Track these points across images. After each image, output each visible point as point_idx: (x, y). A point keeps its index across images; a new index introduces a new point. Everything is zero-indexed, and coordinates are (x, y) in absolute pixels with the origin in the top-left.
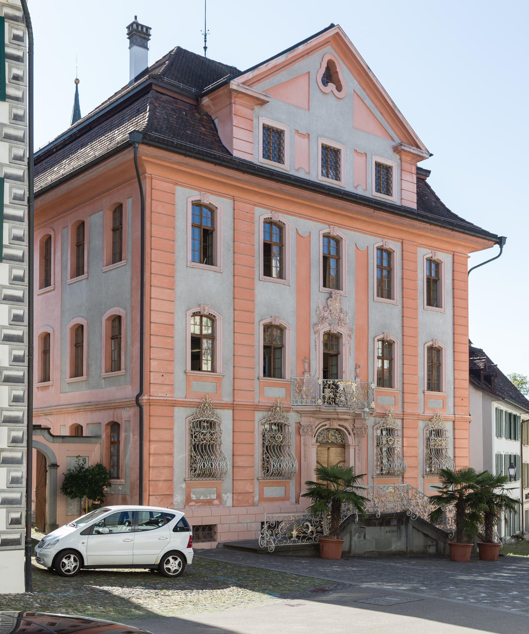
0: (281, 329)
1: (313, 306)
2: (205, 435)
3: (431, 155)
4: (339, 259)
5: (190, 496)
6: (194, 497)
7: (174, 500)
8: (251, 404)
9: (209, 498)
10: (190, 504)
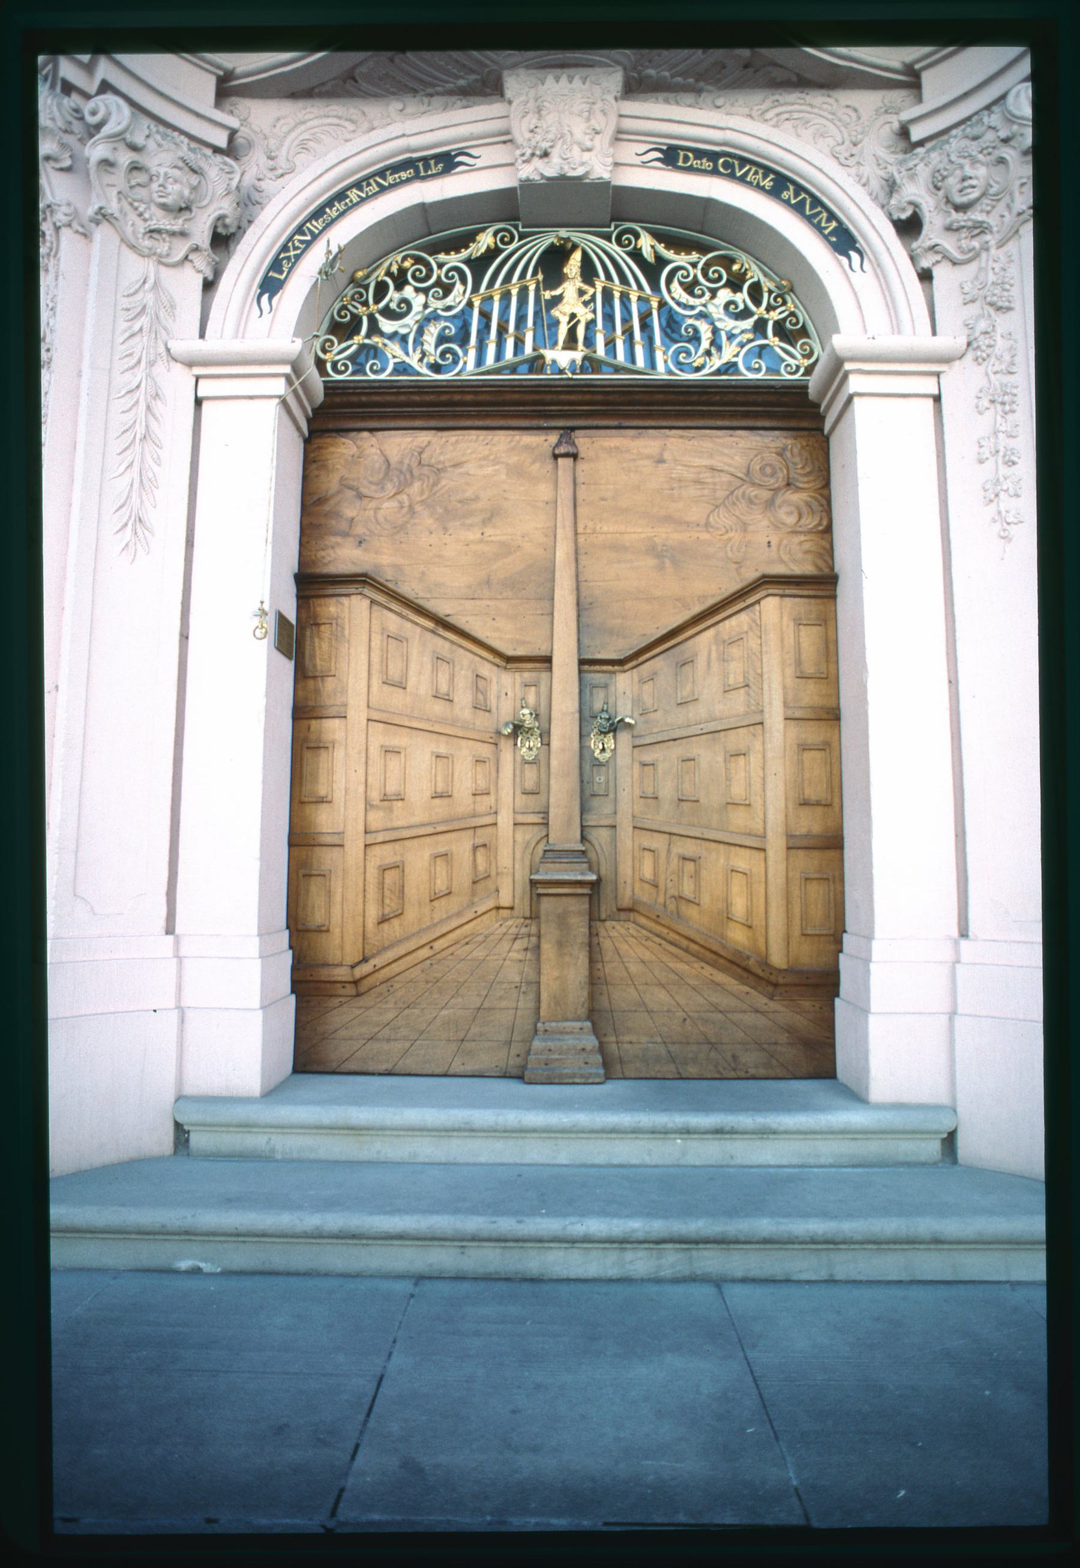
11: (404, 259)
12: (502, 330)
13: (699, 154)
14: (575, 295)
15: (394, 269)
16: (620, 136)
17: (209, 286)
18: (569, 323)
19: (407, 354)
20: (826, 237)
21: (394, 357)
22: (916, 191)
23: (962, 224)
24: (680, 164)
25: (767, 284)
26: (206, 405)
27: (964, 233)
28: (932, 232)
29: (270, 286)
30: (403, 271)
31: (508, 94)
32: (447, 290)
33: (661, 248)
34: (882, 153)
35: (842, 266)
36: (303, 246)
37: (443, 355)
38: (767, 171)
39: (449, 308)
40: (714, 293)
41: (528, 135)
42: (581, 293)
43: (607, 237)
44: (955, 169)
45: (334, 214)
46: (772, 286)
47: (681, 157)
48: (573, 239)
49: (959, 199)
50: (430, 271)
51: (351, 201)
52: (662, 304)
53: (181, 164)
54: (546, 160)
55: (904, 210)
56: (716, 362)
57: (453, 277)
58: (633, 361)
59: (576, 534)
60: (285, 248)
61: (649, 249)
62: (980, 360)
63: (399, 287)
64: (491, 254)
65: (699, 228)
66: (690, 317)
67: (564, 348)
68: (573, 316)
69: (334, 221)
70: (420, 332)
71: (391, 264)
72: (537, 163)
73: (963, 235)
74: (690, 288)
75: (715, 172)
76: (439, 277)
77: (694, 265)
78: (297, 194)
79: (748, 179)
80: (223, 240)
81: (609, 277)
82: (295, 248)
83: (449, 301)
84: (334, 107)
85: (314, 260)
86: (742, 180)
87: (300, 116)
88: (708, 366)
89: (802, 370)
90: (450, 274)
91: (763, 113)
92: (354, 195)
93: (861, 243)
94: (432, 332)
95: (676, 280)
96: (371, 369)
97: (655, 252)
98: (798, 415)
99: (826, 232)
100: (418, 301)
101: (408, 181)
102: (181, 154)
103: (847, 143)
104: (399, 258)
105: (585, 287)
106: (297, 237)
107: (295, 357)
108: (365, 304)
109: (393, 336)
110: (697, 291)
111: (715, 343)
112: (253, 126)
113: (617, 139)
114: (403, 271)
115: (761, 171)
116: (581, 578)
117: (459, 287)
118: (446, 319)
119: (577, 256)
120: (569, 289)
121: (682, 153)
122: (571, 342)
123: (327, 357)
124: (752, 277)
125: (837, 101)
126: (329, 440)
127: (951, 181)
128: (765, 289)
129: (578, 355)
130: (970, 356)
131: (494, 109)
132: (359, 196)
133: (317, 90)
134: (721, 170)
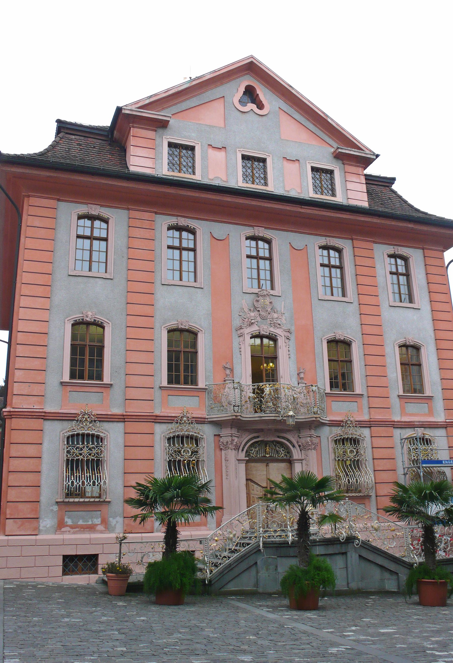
0: (193, 334)
1: (235, 307)
2: (82, 450)
3: (377, 156)
4: (409, 275)
5: (63, 520)
6: (69, 522)
7: (42, 525)
8: (151, 414)
9: (90, 523)
10: (63, 529)
28: (301, 448)
29: (243, 450)
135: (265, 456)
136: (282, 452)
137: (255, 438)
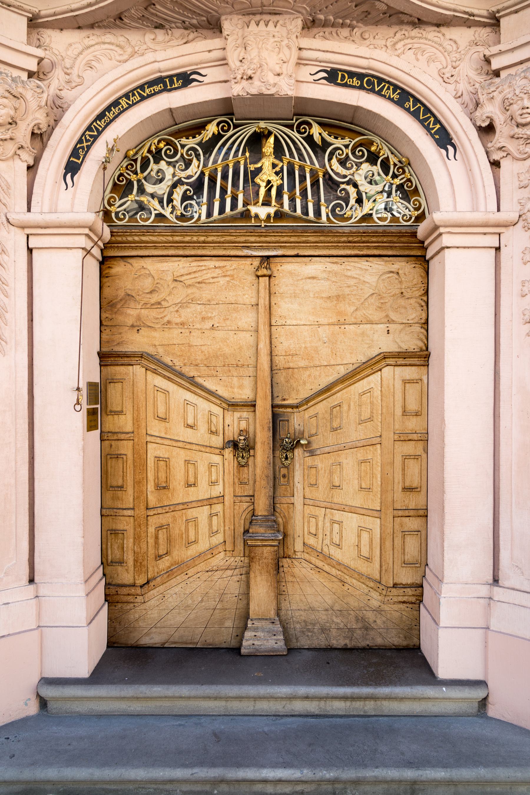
11: (159, 142)
12: (224, 191)
13: (352, 75)
14: (270, 168)
15: (153, 148)
16: (301, 62)
17: (32, 169)
18: (266, 187)
19: (163, 207)
20: (432, 136)
21: (155, 210)
22: (491, 110)
23: (521, 136)
24: (339, 81)
25: (393, 160)
26: (34, 252)
27: (521, 141)
28: (500, 138)
29: (72, 168)
30: (159, 151)
31: (225, 33)
32: (188, 164)
33: (325, 135)
34: (473, 74)
35: (441, 155)
36: (92, 140)
37: (186, 208)
38: (396, 87)
39: (189, 177)
40: (359, 165)
41: (238, 64)
42: (274, 166)
43: (291, 127)
44: (518, 100)
45: (111, 116)
46: (396, 161)
47: (340, 76)
48: (268, 128)
49: (520, 120)
50: (176, 152)
51: (123, 107)
52: (326, 173)
53: (7, 94)
54: (250, 81)
55: (484, 121)
56: (359, 213)
57: (191, 155)
58: (307, 214)
59: (271, 325)
60: (80, 141)
61: (318, 135)
62: (526, 228)
63: (157, 162)
64: (216, 138)
65: (350, 120)
66: (343, 183)
67: (263, 204)
68: (269, 182)
69: (111, 121)
70: (171, 194)
71: (151, 145)
72: (244, 83)
73: (521, 143)
74: (343, 163)
75: (361, 87)
76: (182, 155)
77: (347, 146)
78: (88, 102)
79: (383, 93)
80: (40, 137)
81: (291, 155)
82: (87, 141)
83: (189, 172)
84: (108, 36)
85: (98, 151)
86: (379, 93)
87: (87, 42)
88: (354, 217)
89: (413, 218)
90: (189, 153)
91: (395, 44)
92: (124, 103)
93: (455, 141)
94: (179, 192)
95: (334, 157)
96: (140, 218)
97: (323, 139)
98: (411, 246)
99: (433, 132)
100: (169, 171)
101: (160, 92)
102: (7, 87)
103: (450, 67)
104: (156, 141)
105: (276, 162)
106: (87, 133)
107: (91, 224)
108: (136, 173)
109: (153, 196)
110: (348, 165)
111: (359, 201)
112: (54, 50)
113: (298, 64)
114: (159, 151)
115: (391, 87)
116: (274, 354)
117: (195, 162)
118: (187, 184)
119: (272, 140)
120: (267, 163)
121: (340, 74)
122: (267, 203)
123: (112, 209)
124: (384, 155)
125: (444, 35)
126: (115, 263)
127: (515, 107)
128: (392, 163)
129: (271, 210)
130: (521, 224)
131: (216, 43)
132: (127, 103)
133: (97, 25)
134: (365, 86)
135: (246, 215)
136: (365, 187)
137: (163, 83)
